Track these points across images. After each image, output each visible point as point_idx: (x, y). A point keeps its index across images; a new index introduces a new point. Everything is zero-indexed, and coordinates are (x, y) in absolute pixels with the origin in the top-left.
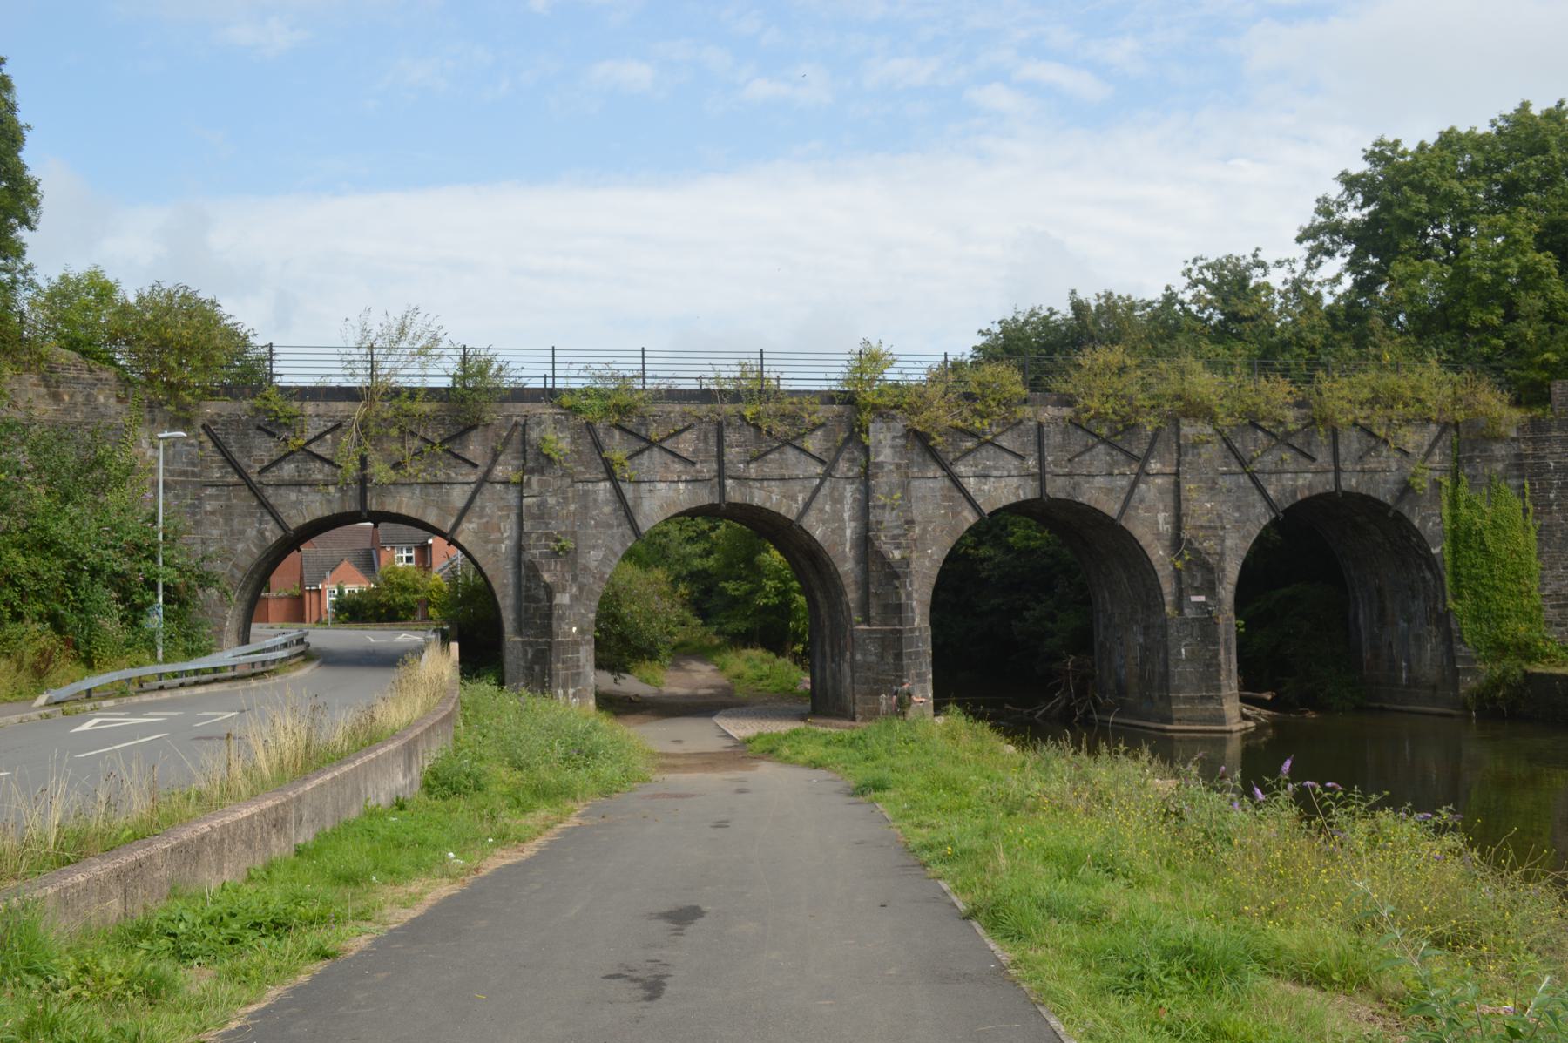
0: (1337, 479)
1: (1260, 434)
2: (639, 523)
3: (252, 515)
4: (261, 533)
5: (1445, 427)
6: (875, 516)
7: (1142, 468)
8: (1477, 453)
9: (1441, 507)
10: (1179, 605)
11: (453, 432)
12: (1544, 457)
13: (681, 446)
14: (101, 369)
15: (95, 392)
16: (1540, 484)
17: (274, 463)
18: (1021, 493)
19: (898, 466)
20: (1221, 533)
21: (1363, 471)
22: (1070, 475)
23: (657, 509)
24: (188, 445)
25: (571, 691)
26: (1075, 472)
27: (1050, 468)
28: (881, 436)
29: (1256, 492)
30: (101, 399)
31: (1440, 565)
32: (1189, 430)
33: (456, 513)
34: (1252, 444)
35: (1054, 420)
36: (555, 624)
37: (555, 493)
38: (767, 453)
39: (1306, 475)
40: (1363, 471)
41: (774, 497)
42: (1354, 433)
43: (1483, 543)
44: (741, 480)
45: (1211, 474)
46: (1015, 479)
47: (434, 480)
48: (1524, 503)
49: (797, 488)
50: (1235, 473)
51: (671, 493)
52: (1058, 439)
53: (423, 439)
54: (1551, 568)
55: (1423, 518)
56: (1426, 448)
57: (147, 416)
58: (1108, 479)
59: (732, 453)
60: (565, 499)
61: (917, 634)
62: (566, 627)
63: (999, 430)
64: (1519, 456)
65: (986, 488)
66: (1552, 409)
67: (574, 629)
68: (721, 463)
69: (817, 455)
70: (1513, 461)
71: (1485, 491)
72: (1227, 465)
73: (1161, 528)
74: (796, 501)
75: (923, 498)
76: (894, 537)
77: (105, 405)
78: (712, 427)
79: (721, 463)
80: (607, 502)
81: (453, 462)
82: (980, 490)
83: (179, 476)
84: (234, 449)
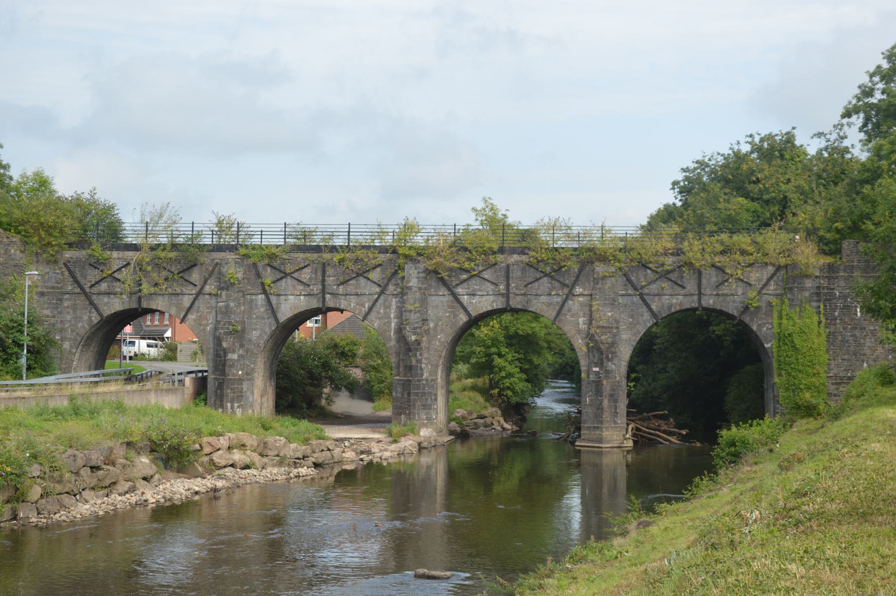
0: (700, 300)
1: (649, 271)
2: (279, 317)
3: (86, 308)
4: (90, 318)
5: (779, 268)
6: (405, 317)
7: (570, 291)
8: (796, 285)
9: (772, 318)
10: (588, 372)
11: (185, 267)
12: (833, 289)
13: (303, 276)
14: (12, 236)
15: (10, 248)
16: (830, 306)
17: (97, 283)
18: (495, 304)
19: (420, 289)
20: (615, 331)
21: (718, 295)
22: (525, 295)
23: (289, 310)
24: (55, 273)
25: (236, 405)
26: (528, 293)
27: (513, 290)
28: (411, 272)
29: (644, 306)
30: (13, 251)
31: (770, 354)
32: (600, 268)
33: (186, 310)
34: (641, 276)
35: (517, 263)
36: (227, 369)
37: (234, 301)
38: (348, 280)
39: (679, 297)
40: (718, 295)
41: (352, 304)
42: (713, 272)
43: (793, 342)
44: (335, 295)
45: (612, 296)
46: (492, 297)
47: (174, 292)
48: (820, 317)
49: (365, 300)
50: (630, 295)
51: (296, 301)
52: (519, 274)
53: (169, 270)
54: (834, 359)
55: (759, 325)
56: (764, 281)
57: (35, 259)
58: (549, 297)
59: (330, 280)
60: (239, 304)
61: (424, 382)
62: (235, 371)
63: (483, 268)
64: (818, 288)
65: (474, 301)
66: (841, 259)
67: (240, 372)
68: (324, 286)
69: (377, 282)
70: (815, 291)
71: (798, 310)
72: (626, 290)
73: (580, 327)
74: (364, 307)
75: (437, 307)
76: (415, 328)
77: (15, 254)
78: (320, 266)
79: (324, 286)
80: (262, 306)
81: (184, 283)
82: (470, 302)
83: (51, 288)
84: (78, 275)
